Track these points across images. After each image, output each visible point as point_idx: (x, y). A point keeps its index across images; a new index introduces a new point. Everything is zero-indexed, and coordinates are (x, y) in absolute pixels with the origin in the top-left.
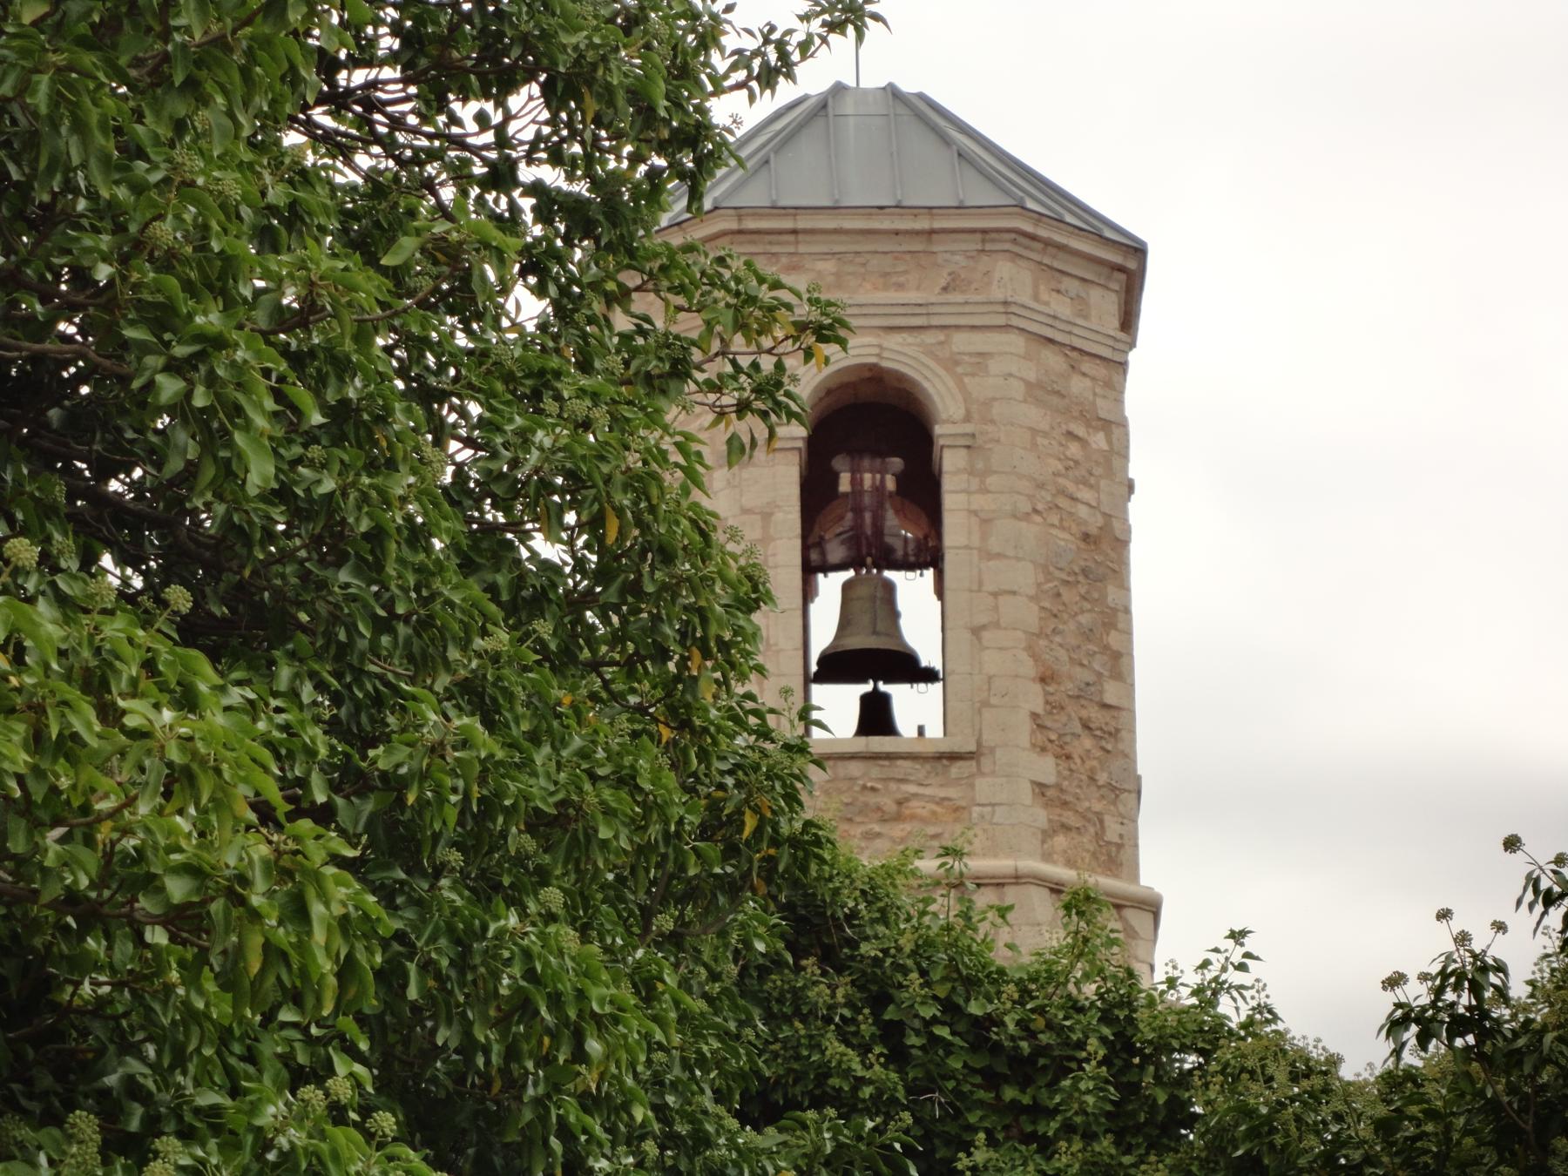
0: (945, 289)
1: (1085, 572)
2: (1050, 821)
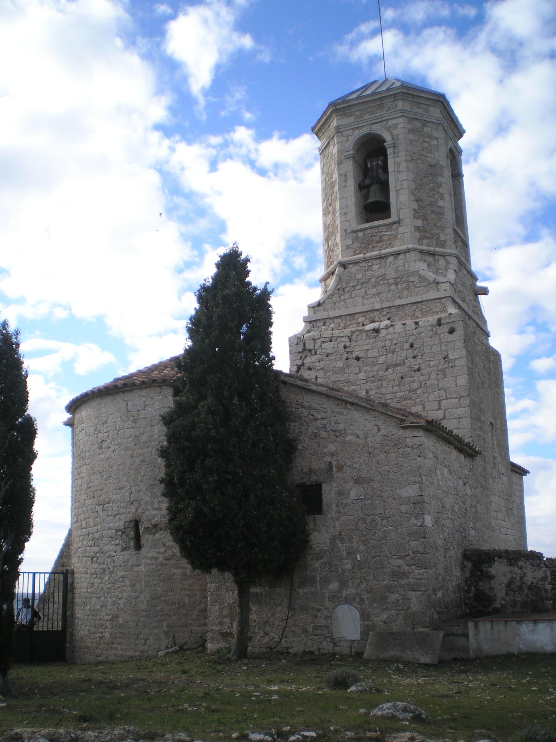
1: (431, 174)
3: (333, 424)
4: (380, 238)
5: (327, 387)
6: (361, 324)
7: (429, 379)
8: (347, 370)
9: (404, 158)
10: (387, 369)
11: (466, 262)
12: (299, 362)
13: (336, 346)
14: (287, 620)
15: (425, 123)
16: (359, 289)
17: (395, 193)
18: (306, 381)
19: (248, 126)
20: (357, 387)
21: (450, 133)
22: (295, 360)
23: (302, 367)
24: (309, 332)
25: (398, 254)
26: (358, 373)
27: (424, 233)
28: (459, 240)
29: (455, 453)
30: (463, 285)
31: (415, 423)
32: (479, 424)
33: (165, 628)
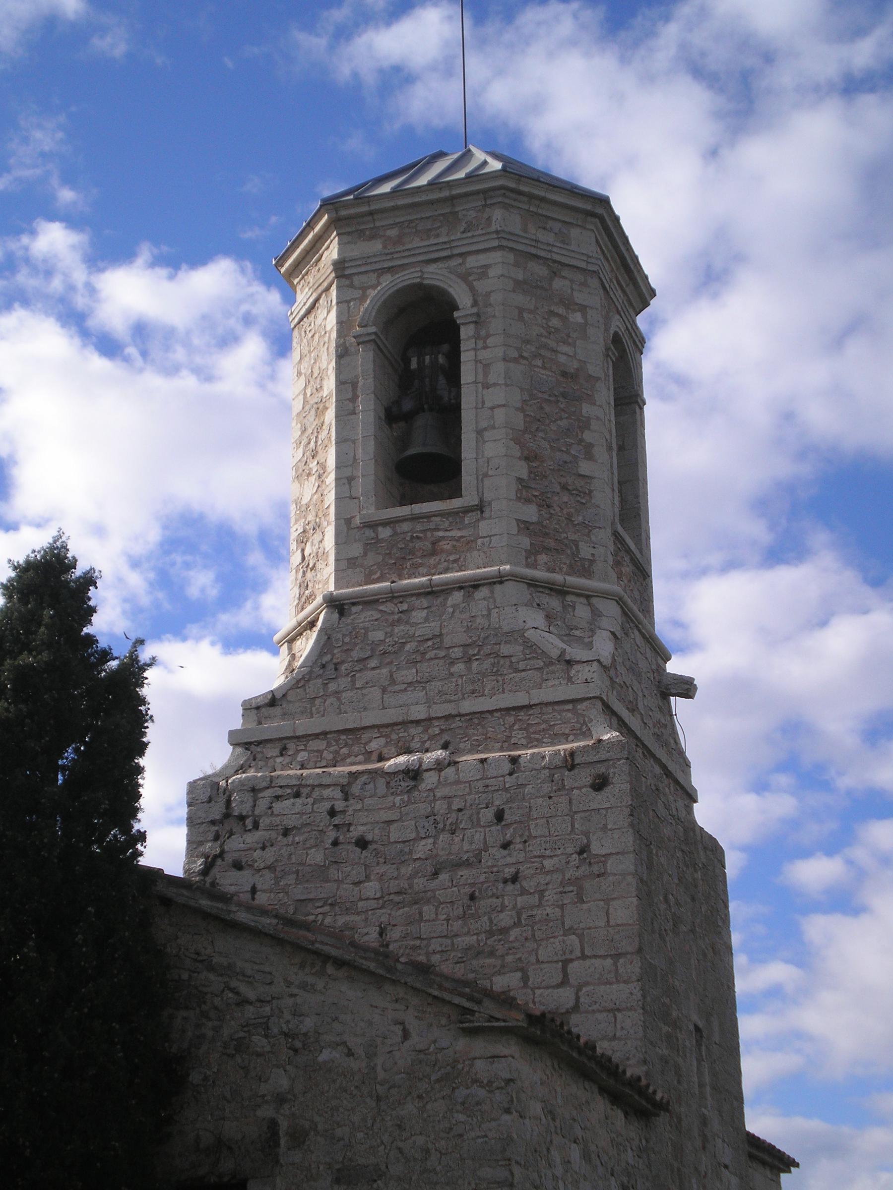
0: (463, 232)
1: (564, 395)
2: (531, 544)
3: (287, 1016)
4: (434, 543)
5: (276, 916)
6: (375, 756)
7: (540, 905)
8: (333, 873)
9: (499, 352)
10: (436, 874)
11: (641, 615)
12: (209, 847)
13: (309, 808)
15: (556, 268)
16: (373, 669)
17: (474, 435)
18: (225, 898)
19: (72, 221)
20: (357, 918)
21: (618, 296)
22: (201, 843)
23: (219, 862)
24: (242, 769)
25: (474, 585)
26: (360, 882)
27: (540, 538)
28: (627, 559)
29: (600, 1106)
30: (633, 669)
31: (498, 1020)
32: (666, 1029)
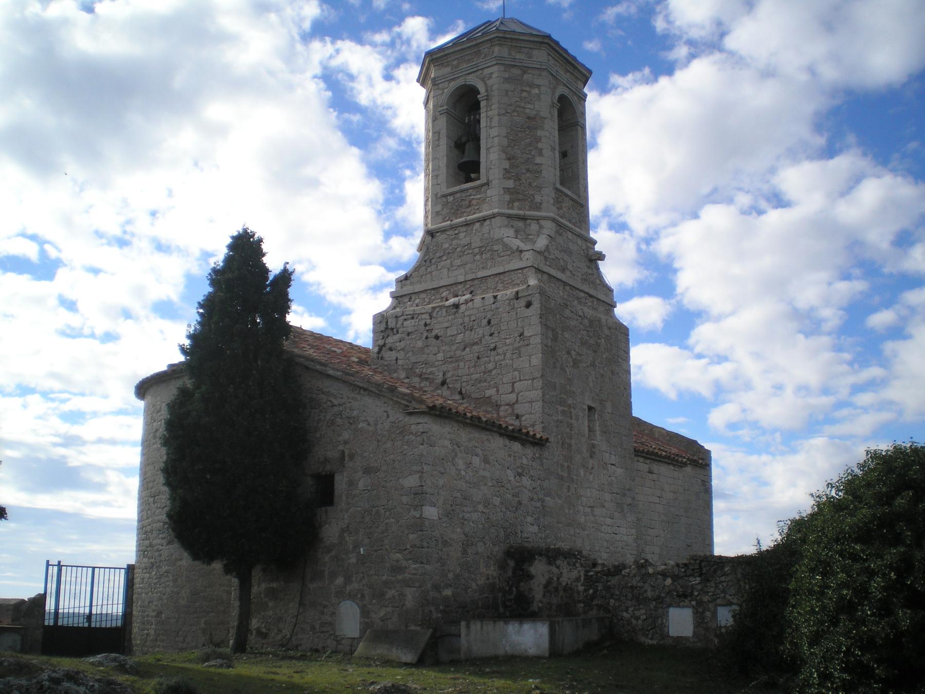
1: (528, 127)
8: (426, 350)
9: (496, 112)
12: (381, 342)
14: (297, 616)
15: (525, 70)
25: (484, 219)
27: (514, 195)
33: (203, 625)
